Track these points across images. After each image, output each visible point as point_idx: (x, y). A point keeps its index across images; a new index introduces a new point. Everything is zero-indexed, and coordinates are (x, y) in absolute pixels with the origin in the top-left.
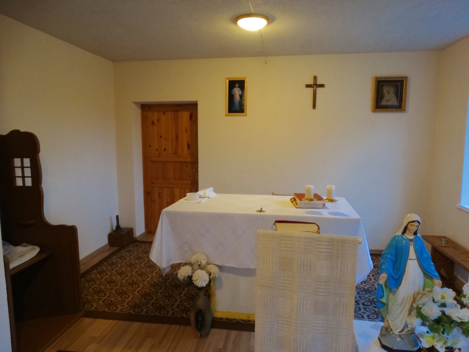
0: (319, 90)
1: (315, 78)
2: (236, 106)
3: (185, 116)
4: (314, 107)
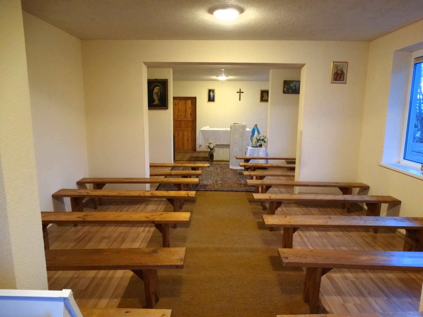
0: (241, 94)
1: (240, 90)
2: (211, 99)
3: (189, 102)
4: (240, 100)
